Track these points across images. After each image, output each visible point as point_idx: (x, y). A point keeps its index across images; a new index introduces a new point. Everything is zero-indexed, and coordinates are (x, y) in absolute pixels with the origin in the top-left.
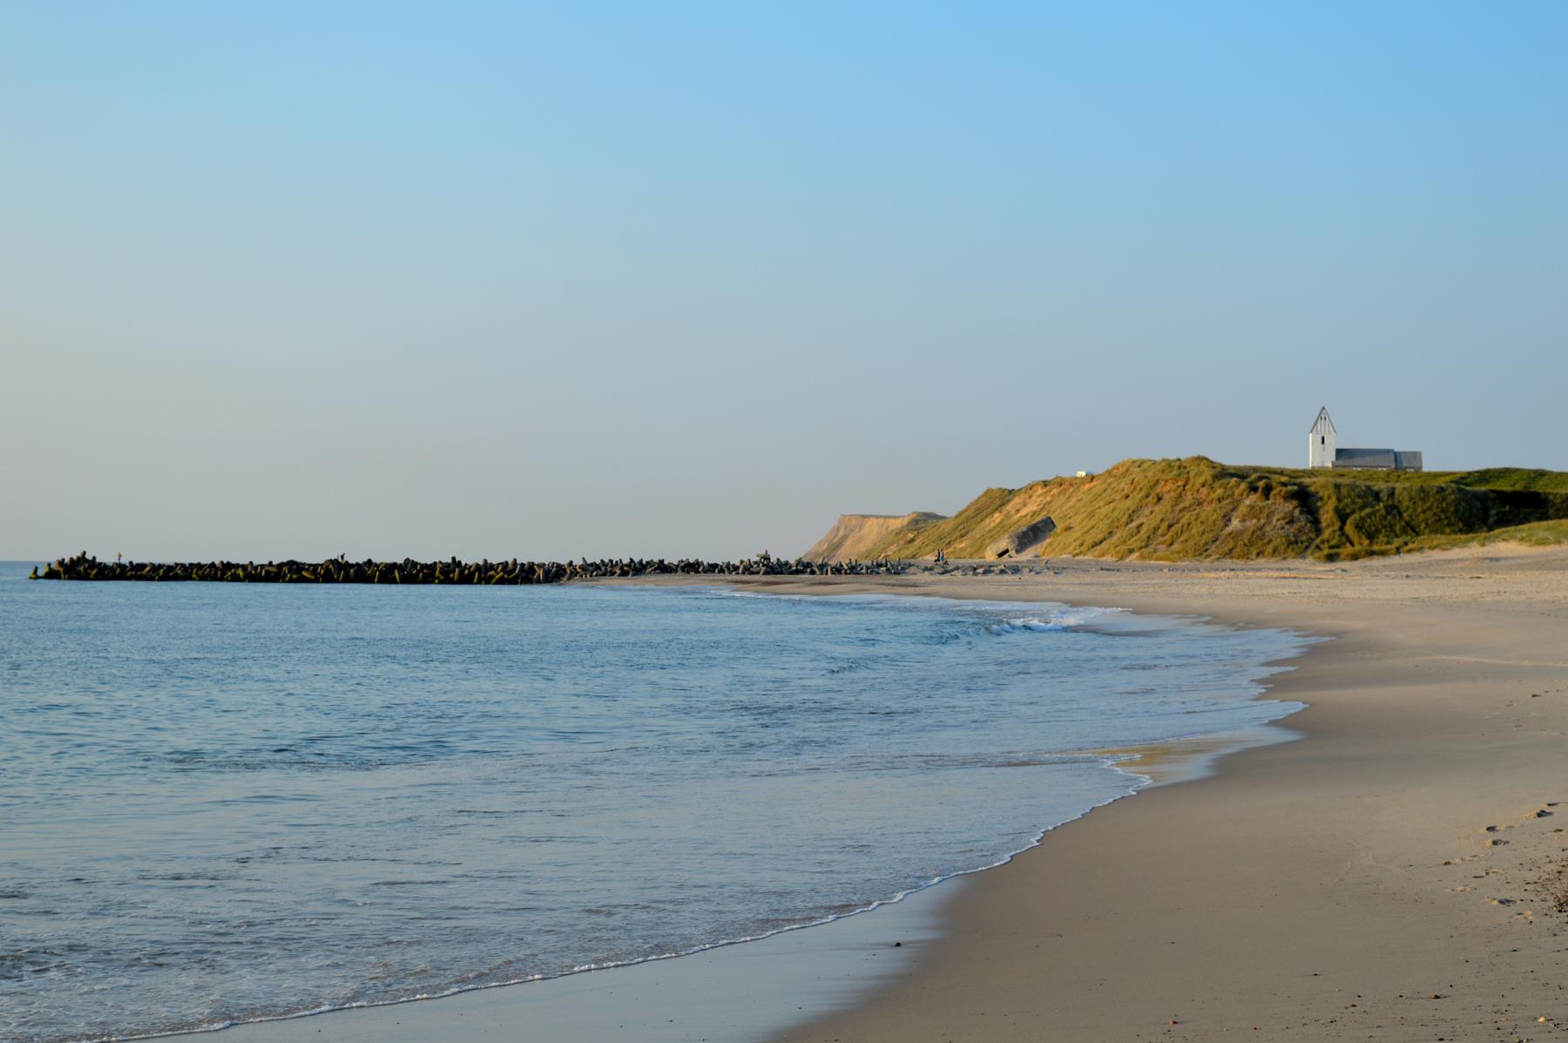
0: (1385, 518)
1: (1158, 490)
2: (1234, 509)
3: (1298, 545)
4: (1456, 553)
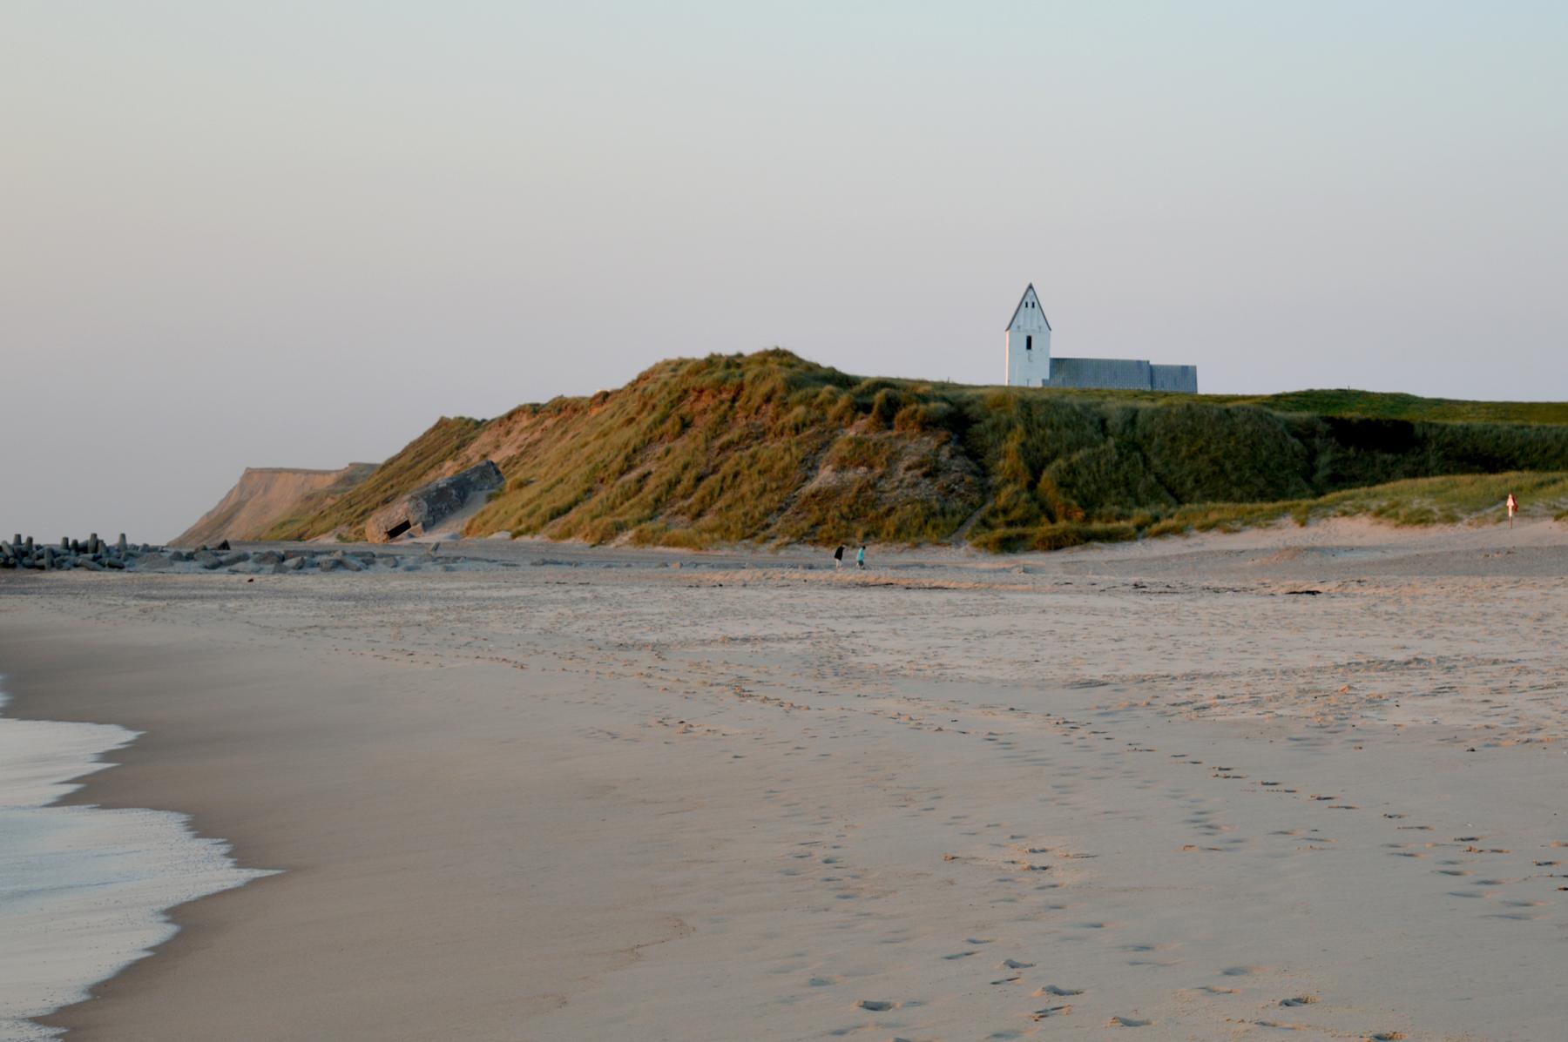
0: (1117, 466)
1: (685, 408)
2: (826, 445)
3: (935, 523)
4: (1250, 539)
